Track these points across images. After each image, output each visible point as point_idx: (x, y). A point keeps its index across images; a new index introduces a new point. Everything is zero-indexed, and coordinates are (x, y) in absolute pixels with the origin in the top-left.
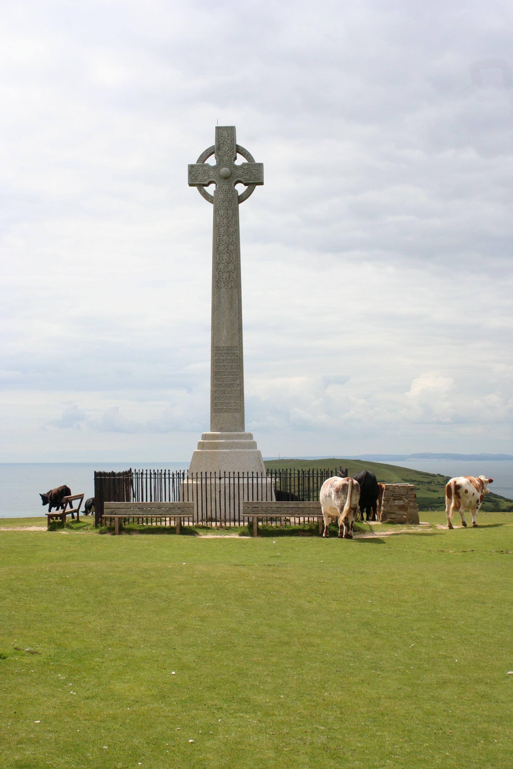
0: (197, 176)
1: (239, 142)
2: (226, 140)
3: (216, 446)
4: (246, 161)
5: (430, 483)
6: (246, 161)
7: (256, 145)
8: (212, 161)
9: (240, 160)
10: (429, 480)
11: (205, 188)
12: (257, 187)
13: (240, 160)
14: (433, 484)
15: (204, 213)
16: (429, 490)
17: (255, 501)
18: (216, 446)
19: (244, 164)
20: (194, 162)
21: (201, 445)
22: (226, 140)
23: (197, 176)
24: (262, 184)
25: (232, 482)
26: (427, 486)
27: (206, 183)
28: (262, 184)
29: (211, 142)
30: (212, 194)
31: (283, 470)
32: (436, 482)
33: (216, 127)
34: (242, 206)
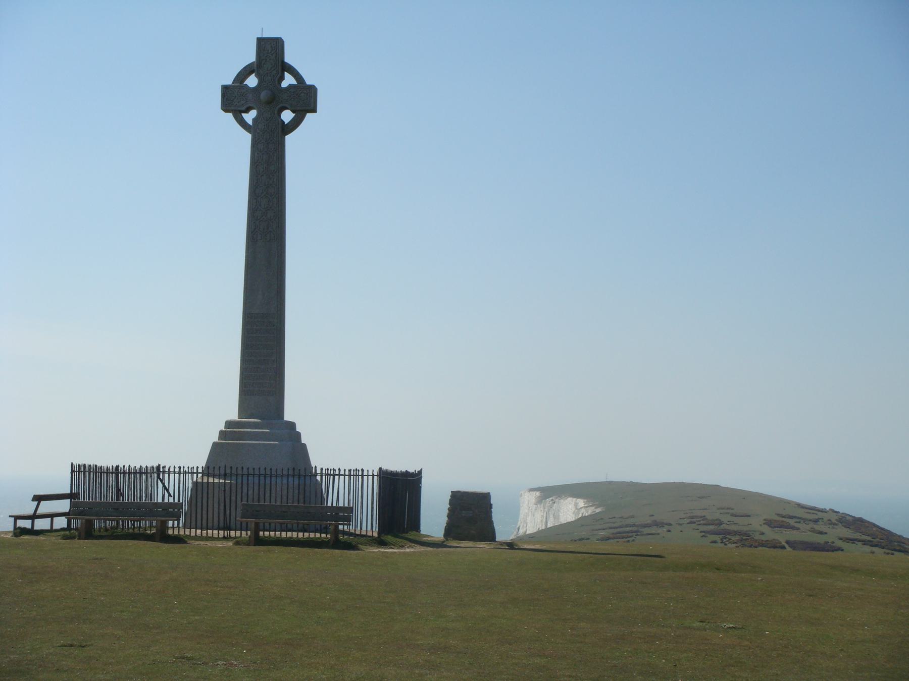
0: (233, 99)
1: (287, 59)
2: (270, 53)
3: (242, 436)
4: (294, 82)
5: (816, 521)
6: (294, 82)
7: (304, 59)
8: (252, 81)
9: (288, 80)
10: (816, 517)
11: (244, 115)
12: (308, 115)
13: (288, 80)
14: (820, 522)
15: (235, 144)
16: (813, 531)
17: (278, 504)
18: (242, 436)
19: (290, 86)
20: (229, 82)
21: (222, 434)
22: (270, 53)
23: (233, 99)
24: (314, 110)
25: (262, 482)
26: (811, 525)
27: (243, 108)
28: (314, 110)
29: (250, 57)
30: (250, 122)
31: (322, 469)
32: (825, 520)
33: (258, 39)
34: (289, 139)
